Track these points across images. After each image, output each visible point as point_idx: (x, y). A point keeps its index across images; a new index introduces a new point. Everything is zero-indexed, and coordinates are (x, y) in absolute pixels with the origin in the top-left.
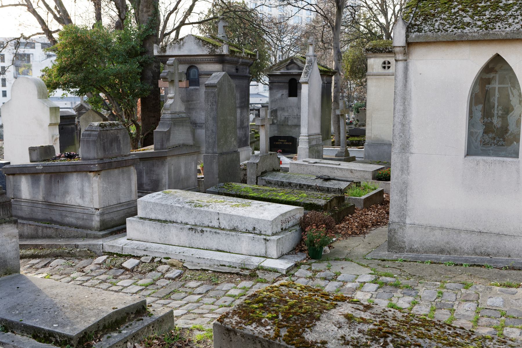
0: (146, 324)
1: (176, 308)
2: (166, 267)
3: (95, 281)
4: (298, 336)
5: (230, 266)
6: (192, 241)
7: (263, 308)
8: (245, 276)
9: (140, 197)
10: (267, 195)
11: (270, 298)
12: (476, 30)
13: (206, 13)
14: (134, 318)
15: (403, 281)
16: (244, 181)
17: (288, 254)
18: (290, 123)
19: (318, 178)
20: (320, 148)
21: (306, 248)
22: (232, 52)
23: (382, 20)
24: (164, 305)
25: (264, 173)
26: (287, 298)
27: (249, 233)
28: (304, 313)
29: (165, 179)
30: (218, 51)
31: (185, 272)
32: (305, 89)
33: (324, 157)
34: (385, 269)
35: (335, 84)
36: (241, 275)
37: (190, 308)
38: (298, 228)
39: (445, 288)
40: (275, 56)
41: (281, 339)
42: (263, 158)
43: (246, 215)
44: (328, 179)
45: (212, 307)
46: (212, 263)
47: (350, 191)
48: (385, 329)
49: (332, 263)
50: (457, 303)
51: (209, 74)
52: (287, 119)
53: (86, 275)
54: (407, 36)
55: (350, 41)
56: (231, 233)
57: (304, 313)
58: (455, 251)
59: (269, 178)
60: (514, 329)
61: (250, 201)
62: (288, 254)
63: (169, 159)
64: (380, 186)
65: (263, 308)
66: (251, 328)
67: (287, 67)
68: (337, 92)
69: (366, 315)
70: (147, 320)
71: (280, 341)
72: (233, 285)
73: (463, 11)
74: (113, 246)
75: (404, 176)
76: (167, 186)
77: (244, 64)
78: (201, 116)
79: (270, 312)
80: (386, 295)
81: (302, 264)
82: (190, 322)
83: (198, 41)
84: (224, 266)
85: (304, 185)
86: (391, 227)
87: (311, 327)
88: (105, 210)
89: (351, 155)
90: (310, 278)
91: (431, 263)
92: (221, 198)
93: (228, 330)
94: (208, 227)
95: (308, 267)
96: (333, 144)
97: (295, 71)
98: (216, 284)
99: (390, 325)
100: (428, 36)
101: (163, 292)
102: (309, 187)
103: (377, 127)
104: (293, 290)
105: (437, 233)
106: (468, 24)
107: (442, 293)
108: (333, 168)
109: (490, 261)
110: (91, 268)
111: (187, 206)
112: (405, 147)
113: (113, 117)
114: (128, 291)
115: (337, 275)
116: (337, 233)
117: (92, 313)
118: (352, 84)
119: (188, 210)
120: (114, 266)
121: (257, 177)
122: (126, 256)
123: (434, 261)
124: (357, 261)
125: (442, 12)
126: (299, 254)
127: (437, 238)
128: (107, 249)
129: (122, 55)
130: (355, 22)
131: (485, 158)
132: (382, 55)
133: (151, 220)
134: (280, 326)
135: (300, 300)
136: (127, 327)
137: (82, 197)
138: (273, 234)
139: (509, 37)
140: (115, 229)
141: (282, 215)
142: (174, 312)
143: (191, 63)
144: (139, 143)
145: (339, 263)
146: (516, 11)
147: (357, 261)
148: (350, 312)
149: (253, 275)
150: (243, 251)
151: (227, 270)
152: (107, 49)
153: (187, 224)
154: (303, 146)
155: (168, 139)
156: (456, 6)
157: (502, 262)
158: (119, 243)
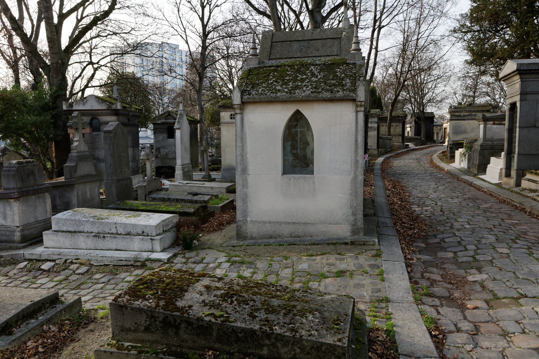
0: (59, 310)
1: (85, 296)
2: (77, 266)
3: (18, 282)
4: (172, 304)
5: (126, 261)
6: (96, 245)
7: (146, 288)
8: (138, 266)
9: (53, 215)
10: (153, 208)
11: (152, 280)
12: (284, 94)
13: (106, 79)
14: (49, 306)
15: (247, 259)
16: (136, 199)
17: (169, 248)
18: (169, 157)
19: (189, 194)
20: (190, 173)
21: (181, 243)
22: (124, 107)
23: (231, 86)
24: (75, 294)
25: (150, 193)
26: (165, 279)
27: (140, 235)
28: (176, 288)
29: (74, 201)
30: (114, 107)
31: (92, 268)
32: (178, 133)
33: (194, 179)
34: (235, 252)
35: (200, 129)
36: (134, 266)
37: (96, 294)
38: (175, 229)
39: (273, 261)
40: (158, 111)
41: (160, 308)
42: (149, 182)
43: (137, 223)
44: (196, 194)
45: (113, 291)
46: (112, 260)
47: (211, 202)
48: (231, 292)
49: (199, 251)
50: (281, 269)
51: (107, 123)
52: (167, 154)
53: (10, 278)
54: (242, 98)
55: (209, 100)
56: (126, 236)
57: (176, 288)
58: (279, 236)
59: (154, 196)
60: (315, 283)
61: (140, 213)
62: (169, 248)
63: (77, 186)
64: (231, 197)
65: (146, 288)
66: (138, 303)
67: (166, 118)
68: (202, 135)
69: (219, 285)
70: (60, 307)
71: (159, 309)
72: (129, 274)
73: (276, 82)
74: (32, 254)
75: (245, 190)
76: (76, 206)
77: (133, 116)
78: (101, 154)
79: (152, 290)
80: (235, 269)
81: (178, 254)
82: (96, 304)
83: (98, 99)
84: (122, 260)
85: (180, 199)
86: (238, 224)
87: (181, 297)
88: (24, 227)
89: (213, 177)
90: (184, 263)
91: (265, 245)
92: (118, 212)
93: (121, 306)
94: (109, 233)
95: (183, 256)
96: (201, 170)
97: (171, 121)
98: (116, 274)
99: (235, 289)
100: (255, 98)
101: (74, 285)
102: (183, 200)
103: (228, 158)
104: (169, 273)
105: (267, 225)
106: (279, 91)
107: (271, 264)
108: (199, 187)
109: (300, 241)
110: (14, 273)
111: (91, 219)
112: (245, 171)
113: (31, 155)
114: (45, 287)
115: (203, 259)
116: (203, 230)
117: (12, 307)
118: (213, 130)
119: (92, 222)
120: (34, 269)
121: (145, 196)
122: (44, 260)
123: (266, 244)
124: (217, 249)
125: (263, 83)
126: (176, 247)
127: (268, 229)
128: (28, 257)
129: (37, 110)
130: (212, 88)
131: (294, 175)
132: (229, 110)
133: (63, 232)
134: (159, 299)
135: (173, 279)
136: (43, 314)
137: (5, 218)
138: (157, 235)
139: (304, 99)
140: (34, 241)
141: (163, 221)
142: (59, 292)
143: (93, 115)
144: (55, 175)
145: (204, 251)
146: (308, 82)
147: (217, 249)
148: (208, 284)
149: (143, 265)
150: (136, 248)
151: (124, 263)
152: (24, 105)
153: (92, 233)
154: (178, 172)
155: (75, 171)
156: (271, 79)
157: (307, 241)
158: (39, 250)
